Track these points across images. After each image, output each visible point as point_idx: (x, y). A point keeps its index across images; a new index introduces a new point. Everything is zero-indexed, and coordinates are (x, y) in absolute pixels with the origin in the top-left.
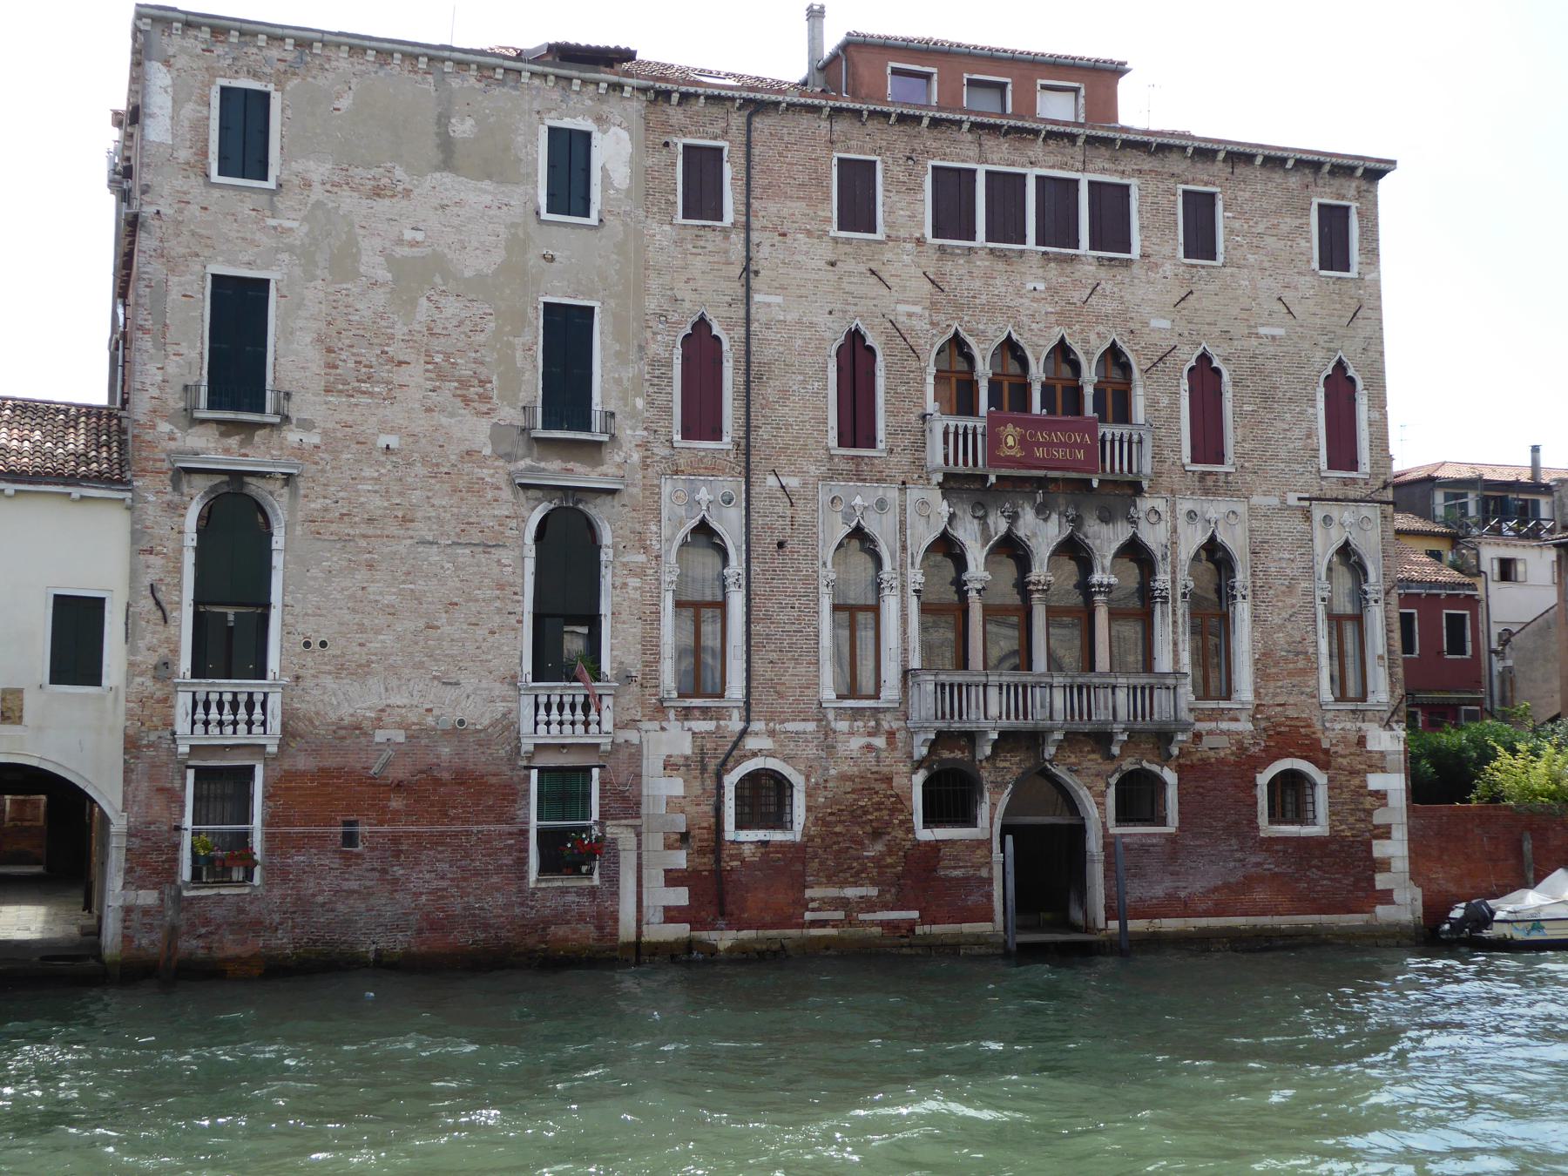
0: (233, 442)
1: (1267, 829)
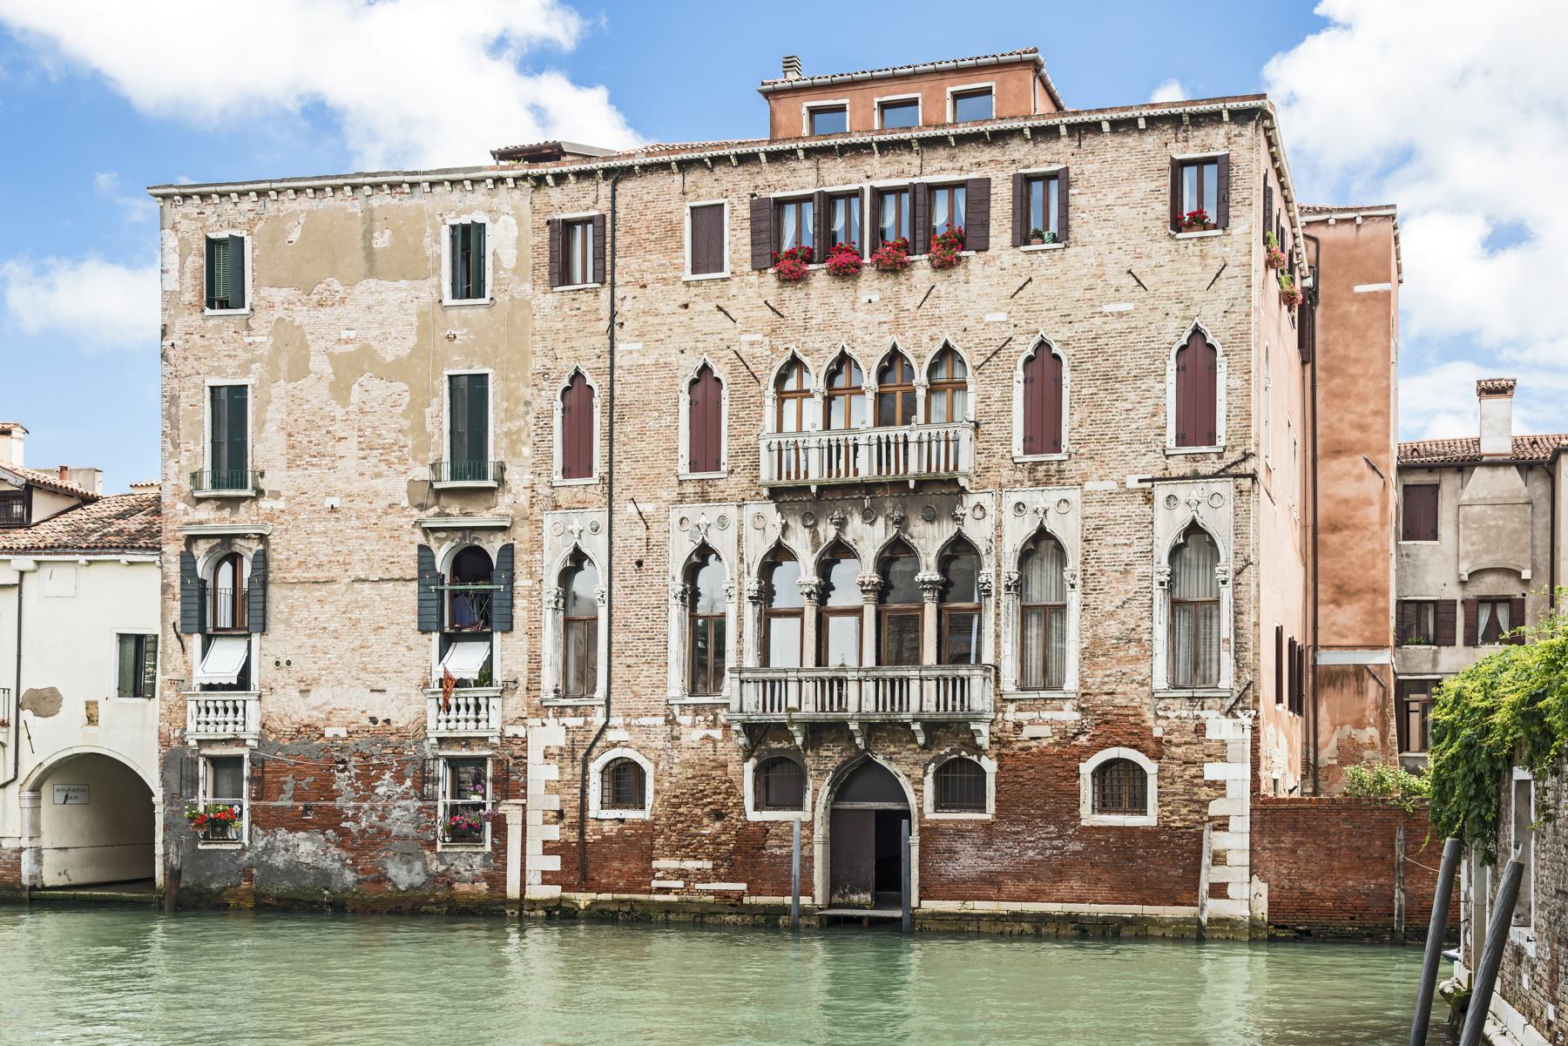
0: (226, 512)
1: (1089, 816)
